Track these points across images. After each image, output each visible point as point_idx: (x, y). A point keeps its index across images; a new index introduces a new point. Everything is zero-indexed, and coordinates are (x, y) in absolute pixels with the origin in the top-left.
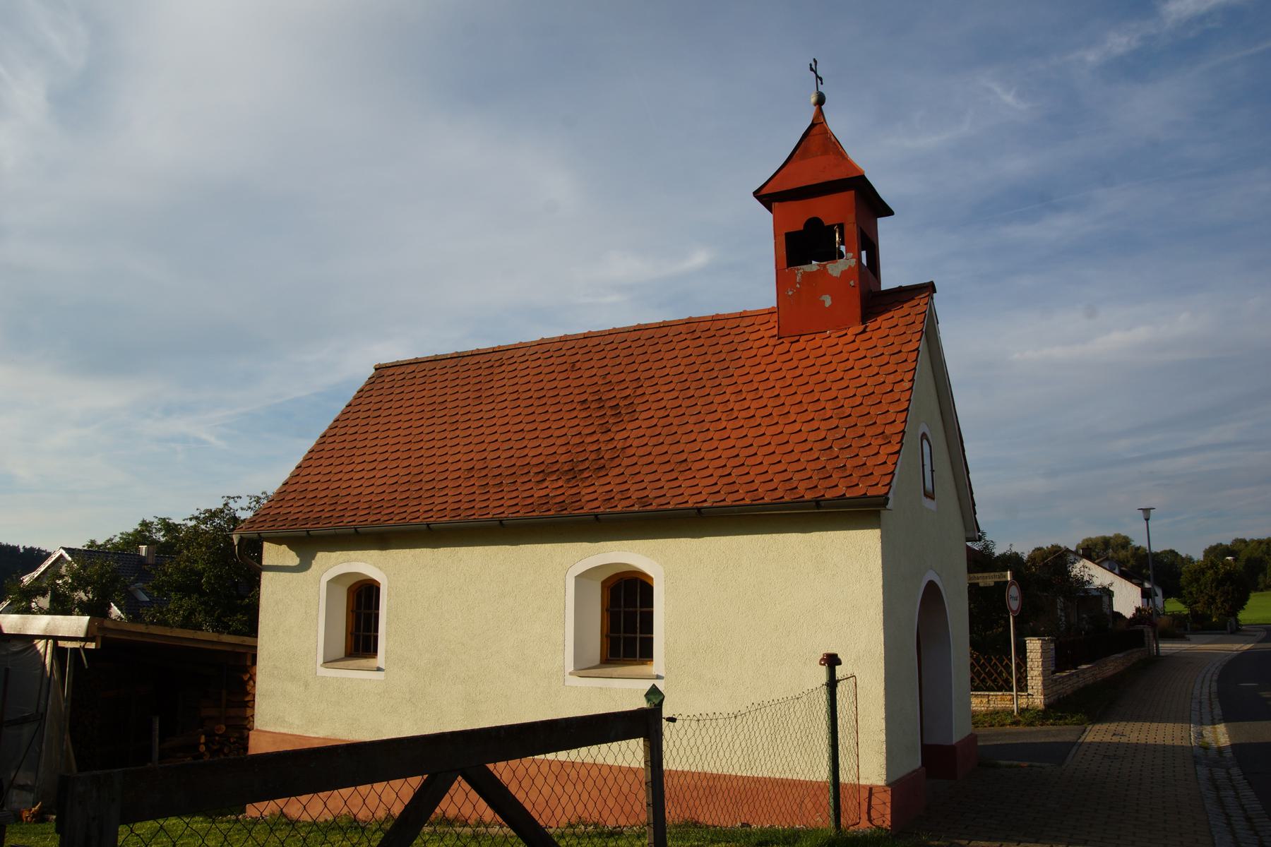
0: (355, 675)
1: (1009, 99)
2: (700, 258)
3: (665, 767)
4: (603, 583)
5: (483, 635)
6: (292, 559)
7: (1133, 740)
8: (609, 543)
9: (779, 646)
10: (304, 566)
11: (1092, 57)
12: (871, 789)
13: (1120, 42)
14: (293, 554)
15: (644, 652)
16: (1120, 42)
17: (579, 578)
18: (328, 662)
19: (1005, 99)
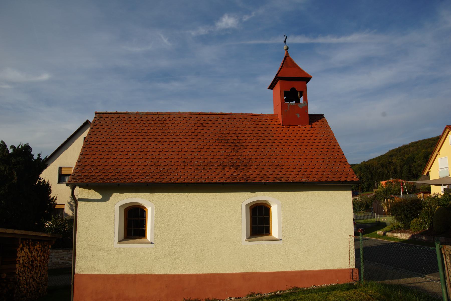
0: (134, 247)
1: (165, 41)
2: (45, 77)
3: (77, 271)
4: (125, 210)
5: (196, 230)
6: (98, 196)
7: (19, 255)
8: (156, 194)
9: (317, 231)
10: (105, 199)
11: (193, 33)
12: (352, 270)
13: (202, 31)
14: (98, 194)
15: (142, 234)
16: (202, 31)
17: (121, 207)
18: (120, 241)
19: (164, 41)
